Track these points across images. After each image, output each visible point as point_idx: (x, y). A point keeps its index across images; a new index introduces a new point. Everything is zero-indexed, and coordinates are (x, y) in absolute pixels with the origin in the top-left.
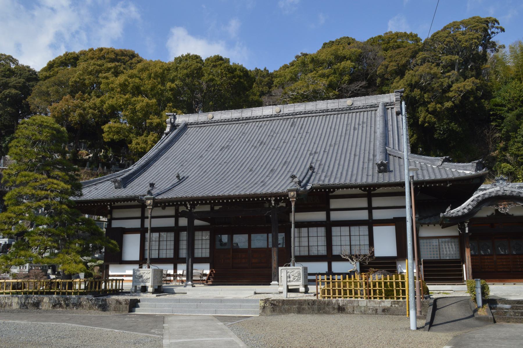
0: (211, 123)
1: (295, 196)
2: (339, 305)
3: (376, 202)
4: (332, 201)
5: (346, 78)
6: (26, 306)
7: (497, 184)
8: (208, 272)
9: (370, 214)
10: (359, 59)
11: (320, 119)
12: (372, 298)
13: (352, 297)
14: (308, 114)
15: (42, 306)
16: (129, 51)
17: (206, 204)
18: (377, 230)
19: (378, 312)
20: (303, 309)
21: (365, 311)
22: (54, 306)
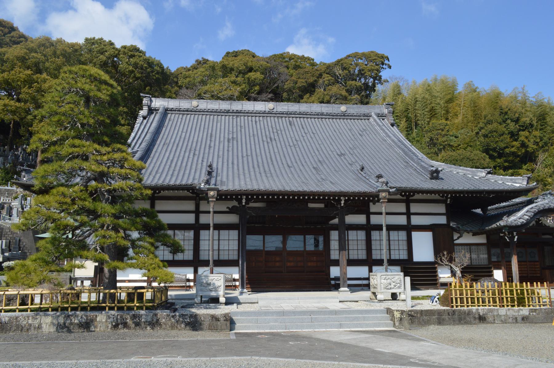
0: (196, 111)
1: (216, 196)
2: (479, 315)
3: (414, 208)
5: (257, 88)
6: (68, 327)
7: (545, 197)
8: (237, 276)
9: (409, 219)
10: (265, 71)
11: (317, 122)
12: (506, 306)
13: (463, 306)
14: (303, 114)
15: (95, 327)
16: (8, 23)
17: (231, 199)
18: (415, 235)
19: (518, 321)
20: (443, 320)
21: (505, 320)
22: (116, 326)
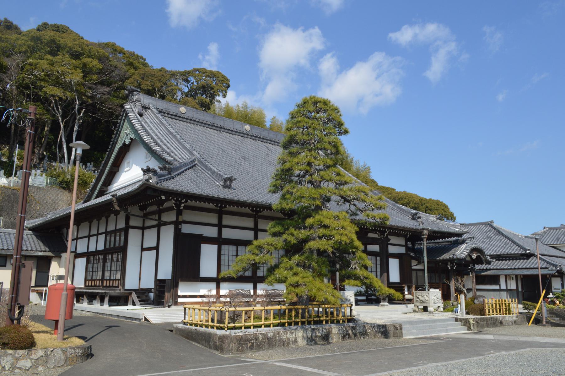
3: (227, 220)
15: (332, 339)
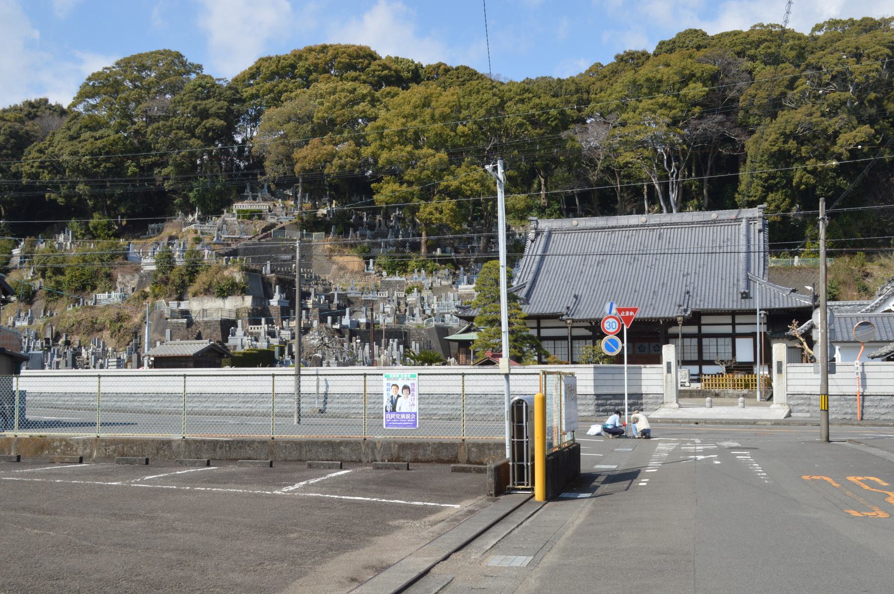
4: (703, 318)
18: (738, 341)
